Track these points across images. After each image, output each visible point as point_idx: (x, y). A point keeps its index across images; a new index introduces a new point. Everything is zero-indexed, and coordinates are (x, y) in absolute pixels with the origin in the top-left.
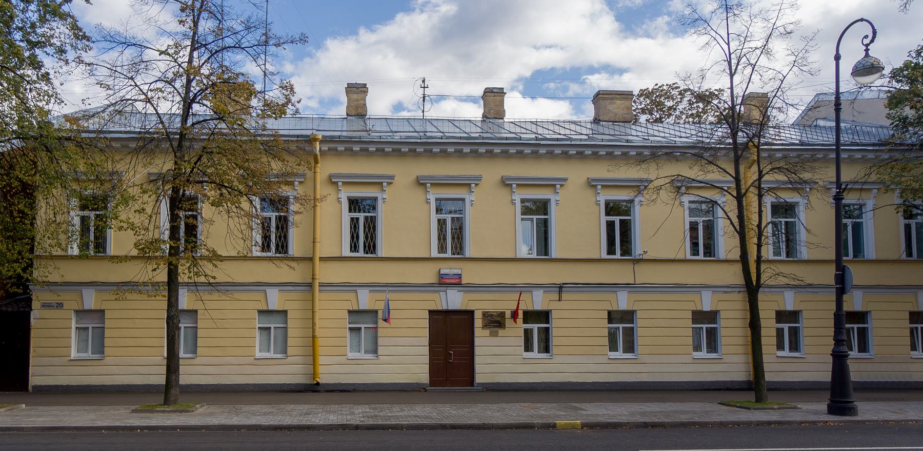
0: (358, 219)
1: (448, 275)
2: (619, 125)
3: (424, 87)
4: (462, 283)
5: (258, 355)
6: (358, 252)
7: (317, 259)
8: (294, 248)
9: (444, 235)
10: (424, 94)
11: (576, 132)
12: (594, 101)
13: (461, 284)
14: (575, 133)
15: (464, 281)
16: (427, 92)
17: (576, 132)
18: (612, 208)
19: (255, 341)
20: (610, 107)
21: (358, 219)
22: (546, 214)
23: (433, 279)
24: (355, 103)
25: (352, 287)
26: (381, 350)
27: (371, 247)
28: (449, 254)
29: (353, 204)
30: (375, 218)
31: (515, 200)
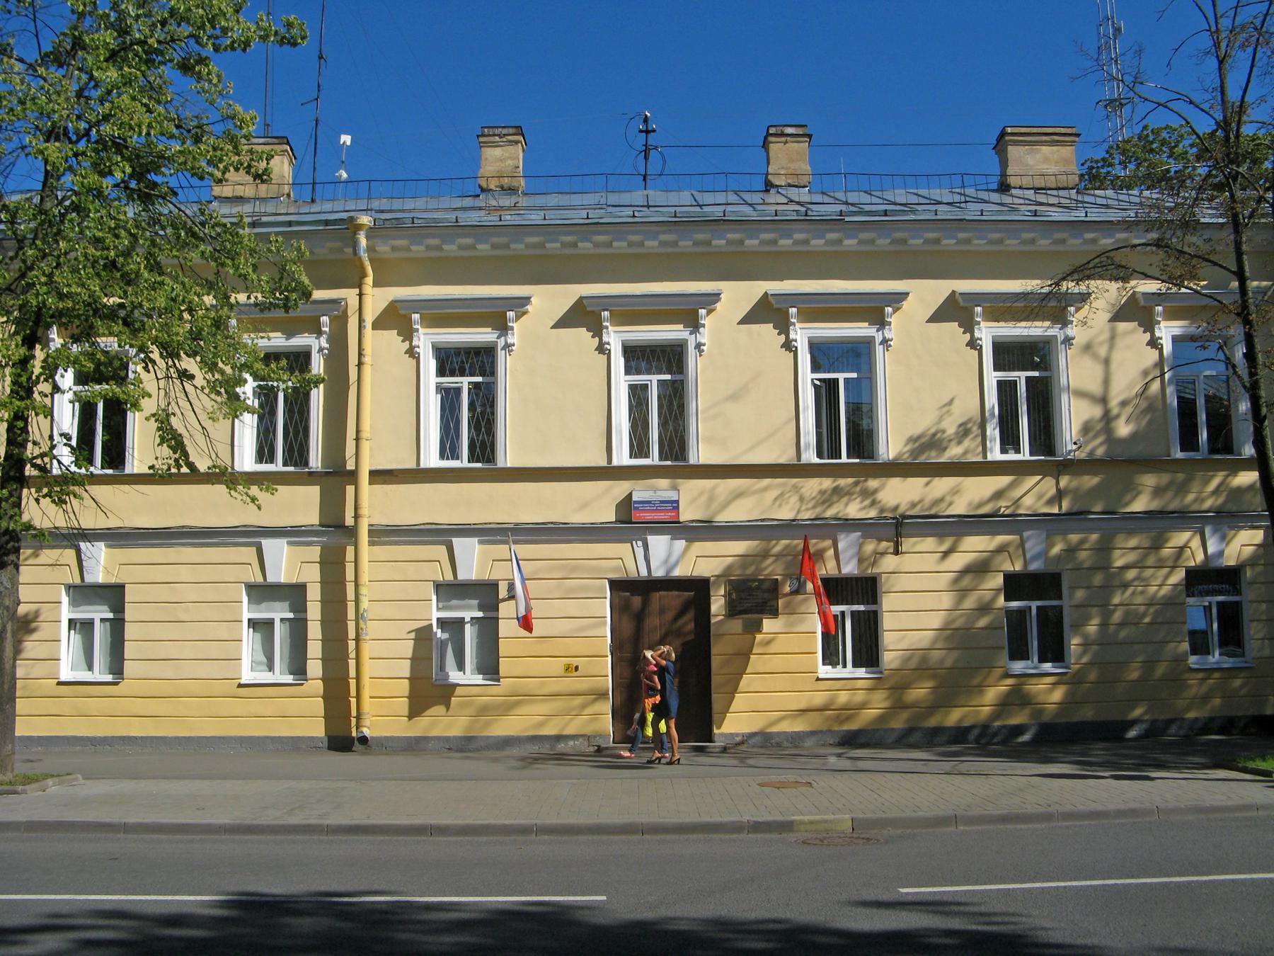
0: (645, 387)
1: (649, 502)
2: (1046, 194)
3: (647, 132)
4: (681, 520)
5: (247, 676)
6: (458, 459)
7: (364, 477)
8: (316, 460)
9: (301, 444)
10: (646, 145)
11: (883, 199)
12: (998, 148)
13: (679, 522)
14: (881, 201)
15: (686, 515)
16: (652, 139)
17: (883, 199)
18: (1007, 354)
19: (240, 650)
20: (1030, 160)
21: (645, 387)
22: (1046, 369)
23: (607, 514)
24: (498, 164)
25: (442, 534)
26: (504, 666)
27: (484, 448)
28: (654, 459)
29: (296, 362)
30: (683, 384)
31: (419, 347)
